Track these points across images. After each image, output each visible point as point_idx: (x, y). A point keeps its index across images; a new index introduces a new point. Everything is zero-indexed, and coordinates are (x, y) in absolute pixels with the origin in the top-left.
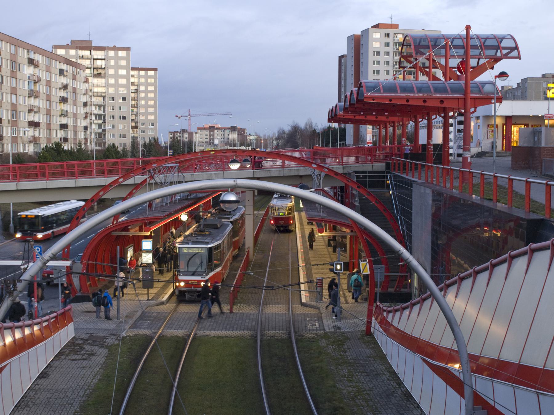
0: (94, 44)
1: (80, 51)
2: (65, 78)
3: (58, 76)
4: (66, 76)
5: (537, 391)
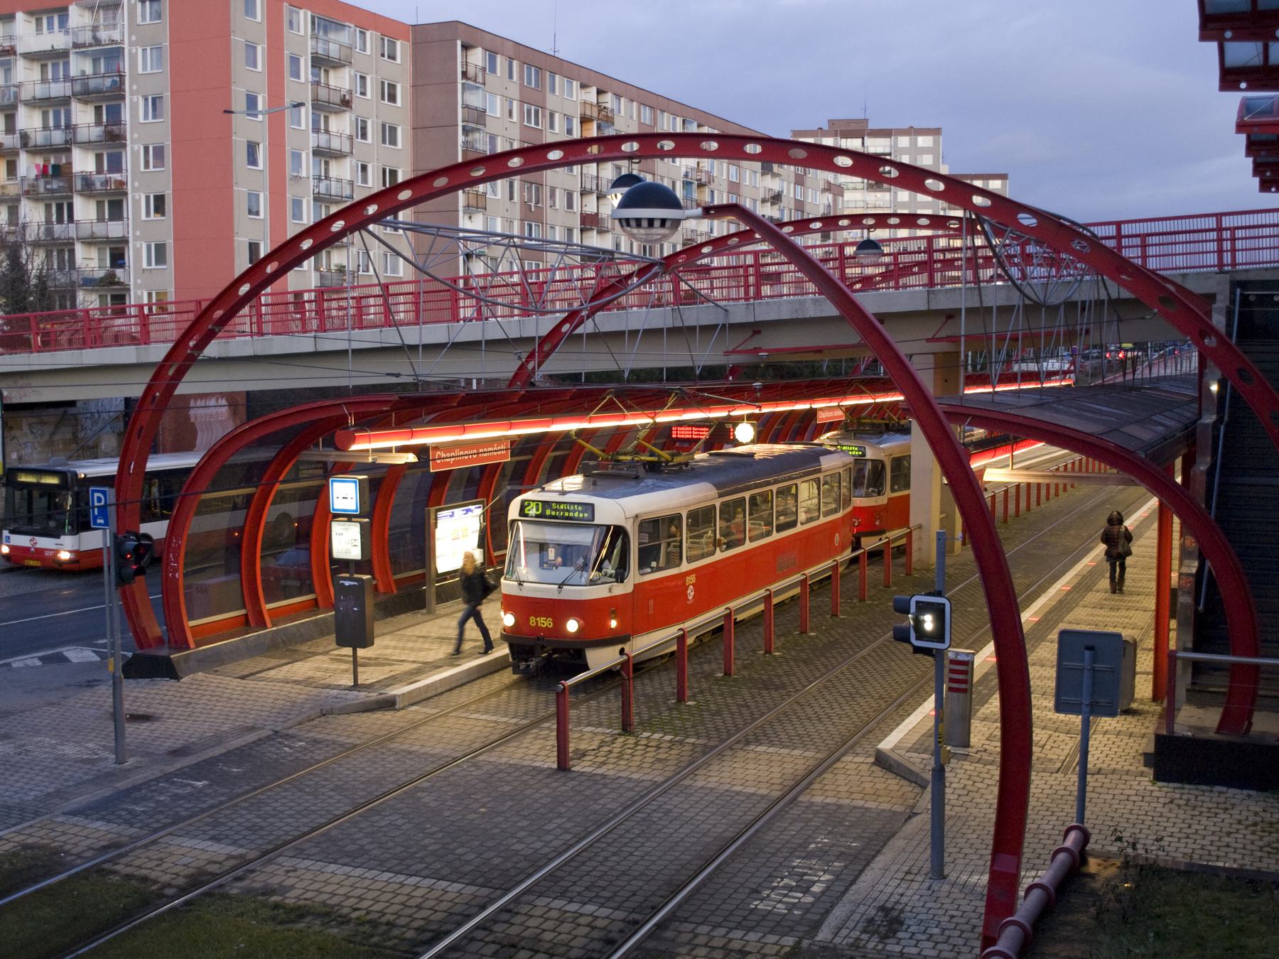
0: (872, 126)
1: (844, 140)
2: (777, 179)
3: (759, 175)
4: (778, 175)
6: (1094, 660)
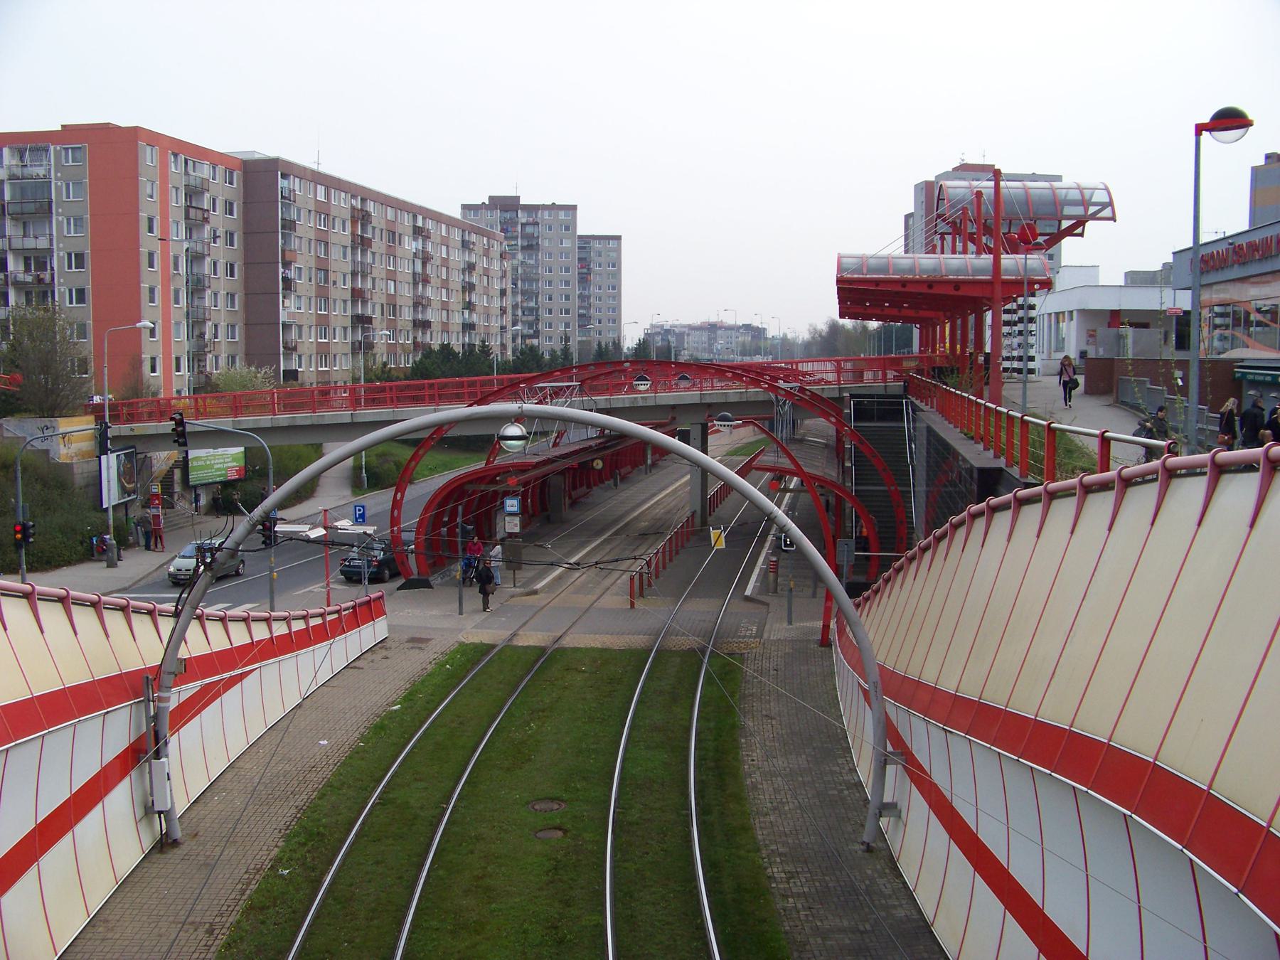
5: (945, 727)
6: (848, 547)
